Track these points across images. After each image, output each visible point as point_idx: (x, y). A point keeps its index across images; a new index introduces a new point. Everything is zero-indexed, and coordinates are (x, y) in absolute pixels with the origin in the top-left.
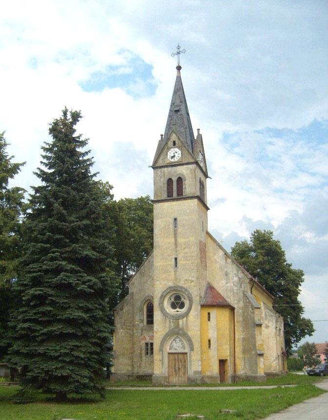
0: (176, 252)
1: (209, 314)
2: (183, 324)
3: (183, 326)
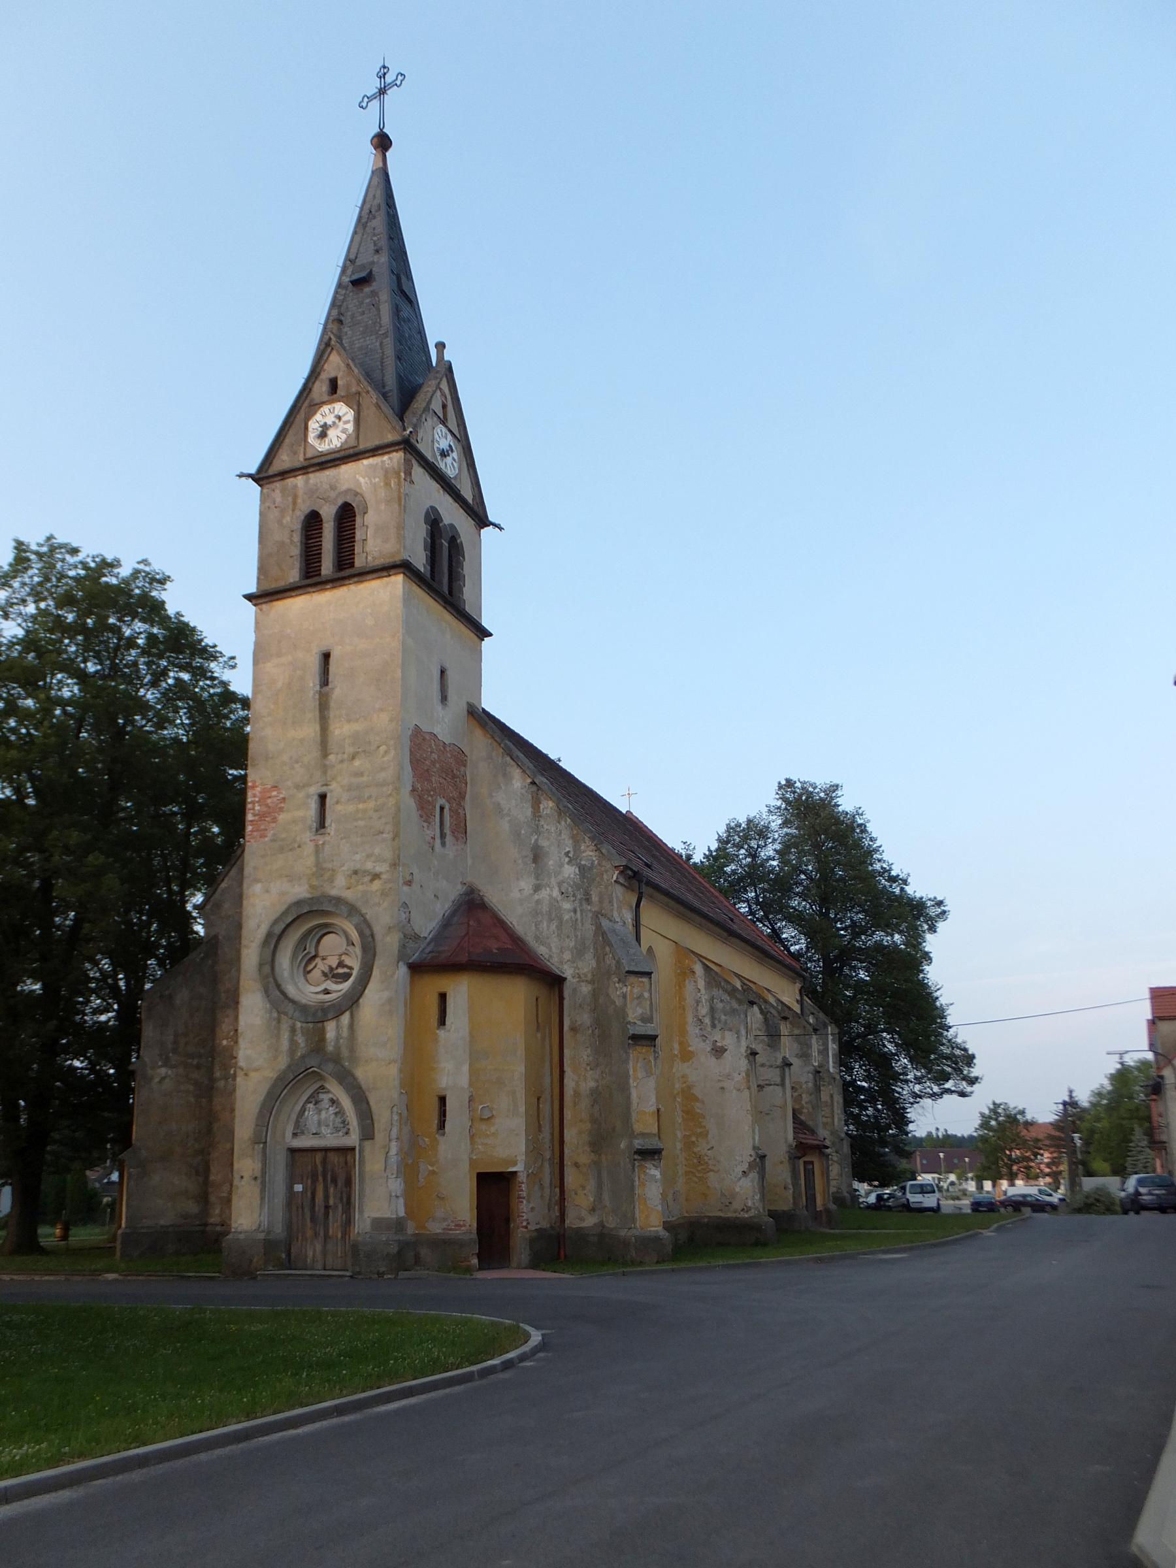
0: (325, 772)
1: (443, 997)
2: (338, 1037)
3: (337, 1047)
